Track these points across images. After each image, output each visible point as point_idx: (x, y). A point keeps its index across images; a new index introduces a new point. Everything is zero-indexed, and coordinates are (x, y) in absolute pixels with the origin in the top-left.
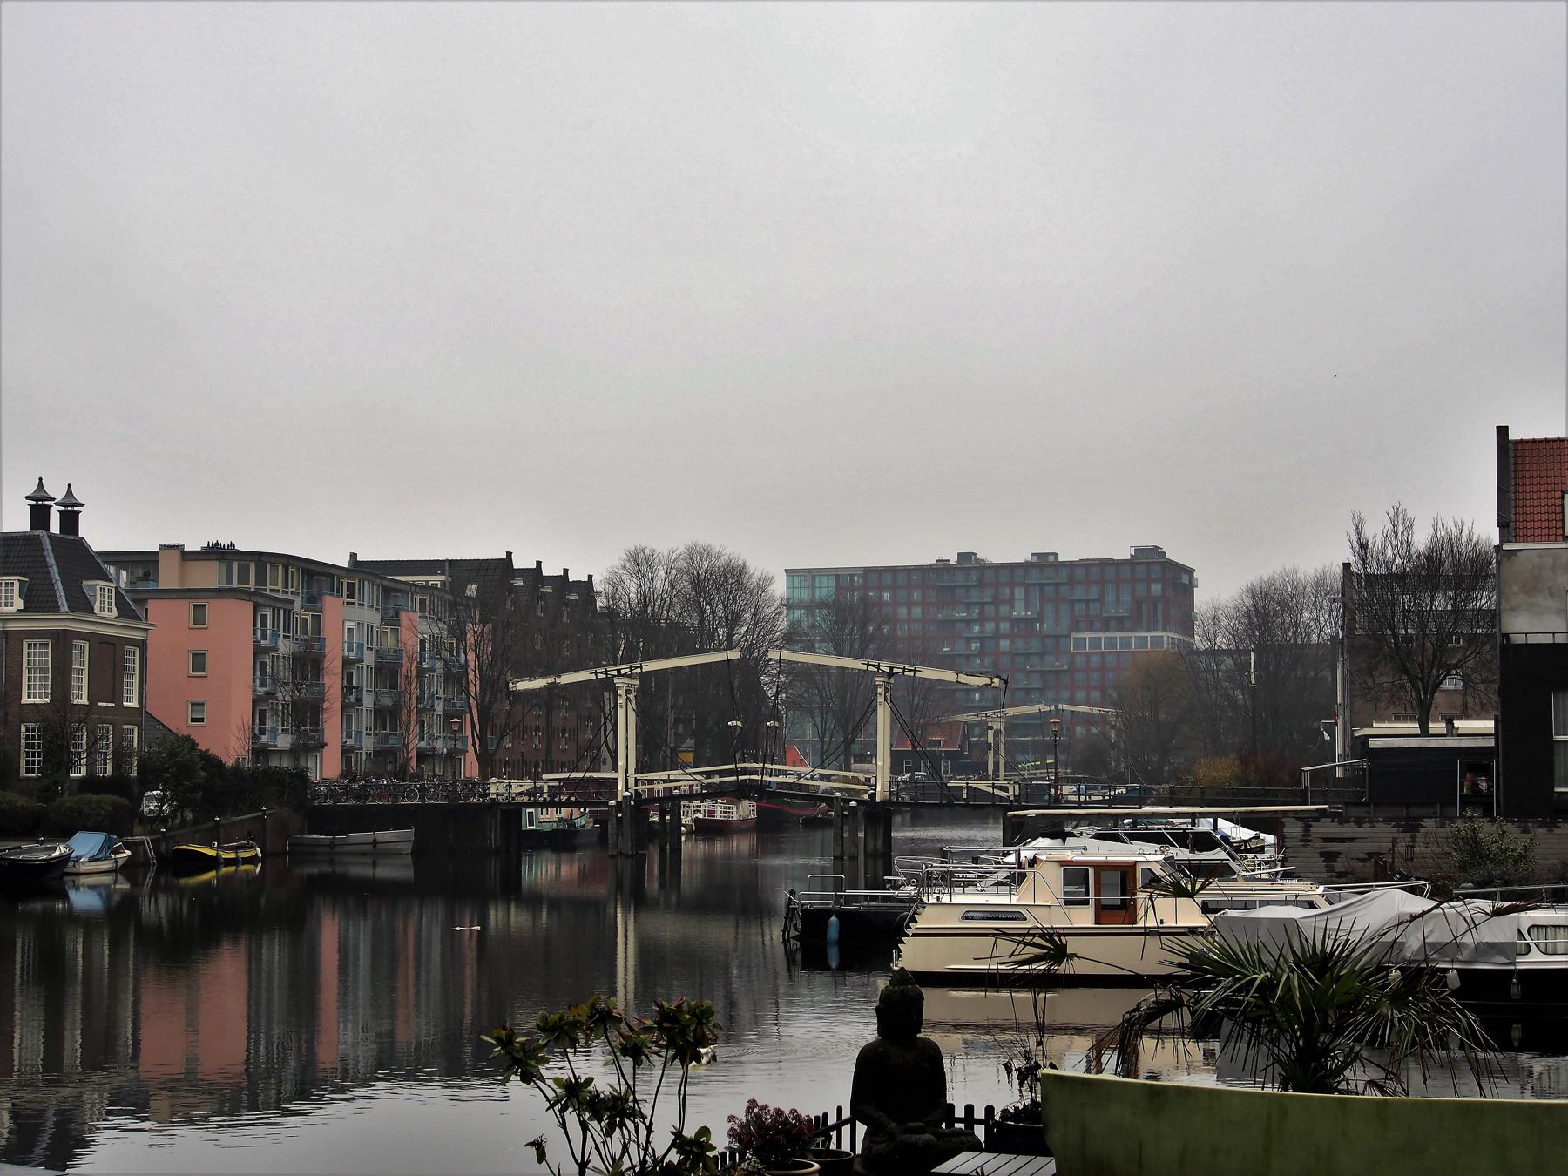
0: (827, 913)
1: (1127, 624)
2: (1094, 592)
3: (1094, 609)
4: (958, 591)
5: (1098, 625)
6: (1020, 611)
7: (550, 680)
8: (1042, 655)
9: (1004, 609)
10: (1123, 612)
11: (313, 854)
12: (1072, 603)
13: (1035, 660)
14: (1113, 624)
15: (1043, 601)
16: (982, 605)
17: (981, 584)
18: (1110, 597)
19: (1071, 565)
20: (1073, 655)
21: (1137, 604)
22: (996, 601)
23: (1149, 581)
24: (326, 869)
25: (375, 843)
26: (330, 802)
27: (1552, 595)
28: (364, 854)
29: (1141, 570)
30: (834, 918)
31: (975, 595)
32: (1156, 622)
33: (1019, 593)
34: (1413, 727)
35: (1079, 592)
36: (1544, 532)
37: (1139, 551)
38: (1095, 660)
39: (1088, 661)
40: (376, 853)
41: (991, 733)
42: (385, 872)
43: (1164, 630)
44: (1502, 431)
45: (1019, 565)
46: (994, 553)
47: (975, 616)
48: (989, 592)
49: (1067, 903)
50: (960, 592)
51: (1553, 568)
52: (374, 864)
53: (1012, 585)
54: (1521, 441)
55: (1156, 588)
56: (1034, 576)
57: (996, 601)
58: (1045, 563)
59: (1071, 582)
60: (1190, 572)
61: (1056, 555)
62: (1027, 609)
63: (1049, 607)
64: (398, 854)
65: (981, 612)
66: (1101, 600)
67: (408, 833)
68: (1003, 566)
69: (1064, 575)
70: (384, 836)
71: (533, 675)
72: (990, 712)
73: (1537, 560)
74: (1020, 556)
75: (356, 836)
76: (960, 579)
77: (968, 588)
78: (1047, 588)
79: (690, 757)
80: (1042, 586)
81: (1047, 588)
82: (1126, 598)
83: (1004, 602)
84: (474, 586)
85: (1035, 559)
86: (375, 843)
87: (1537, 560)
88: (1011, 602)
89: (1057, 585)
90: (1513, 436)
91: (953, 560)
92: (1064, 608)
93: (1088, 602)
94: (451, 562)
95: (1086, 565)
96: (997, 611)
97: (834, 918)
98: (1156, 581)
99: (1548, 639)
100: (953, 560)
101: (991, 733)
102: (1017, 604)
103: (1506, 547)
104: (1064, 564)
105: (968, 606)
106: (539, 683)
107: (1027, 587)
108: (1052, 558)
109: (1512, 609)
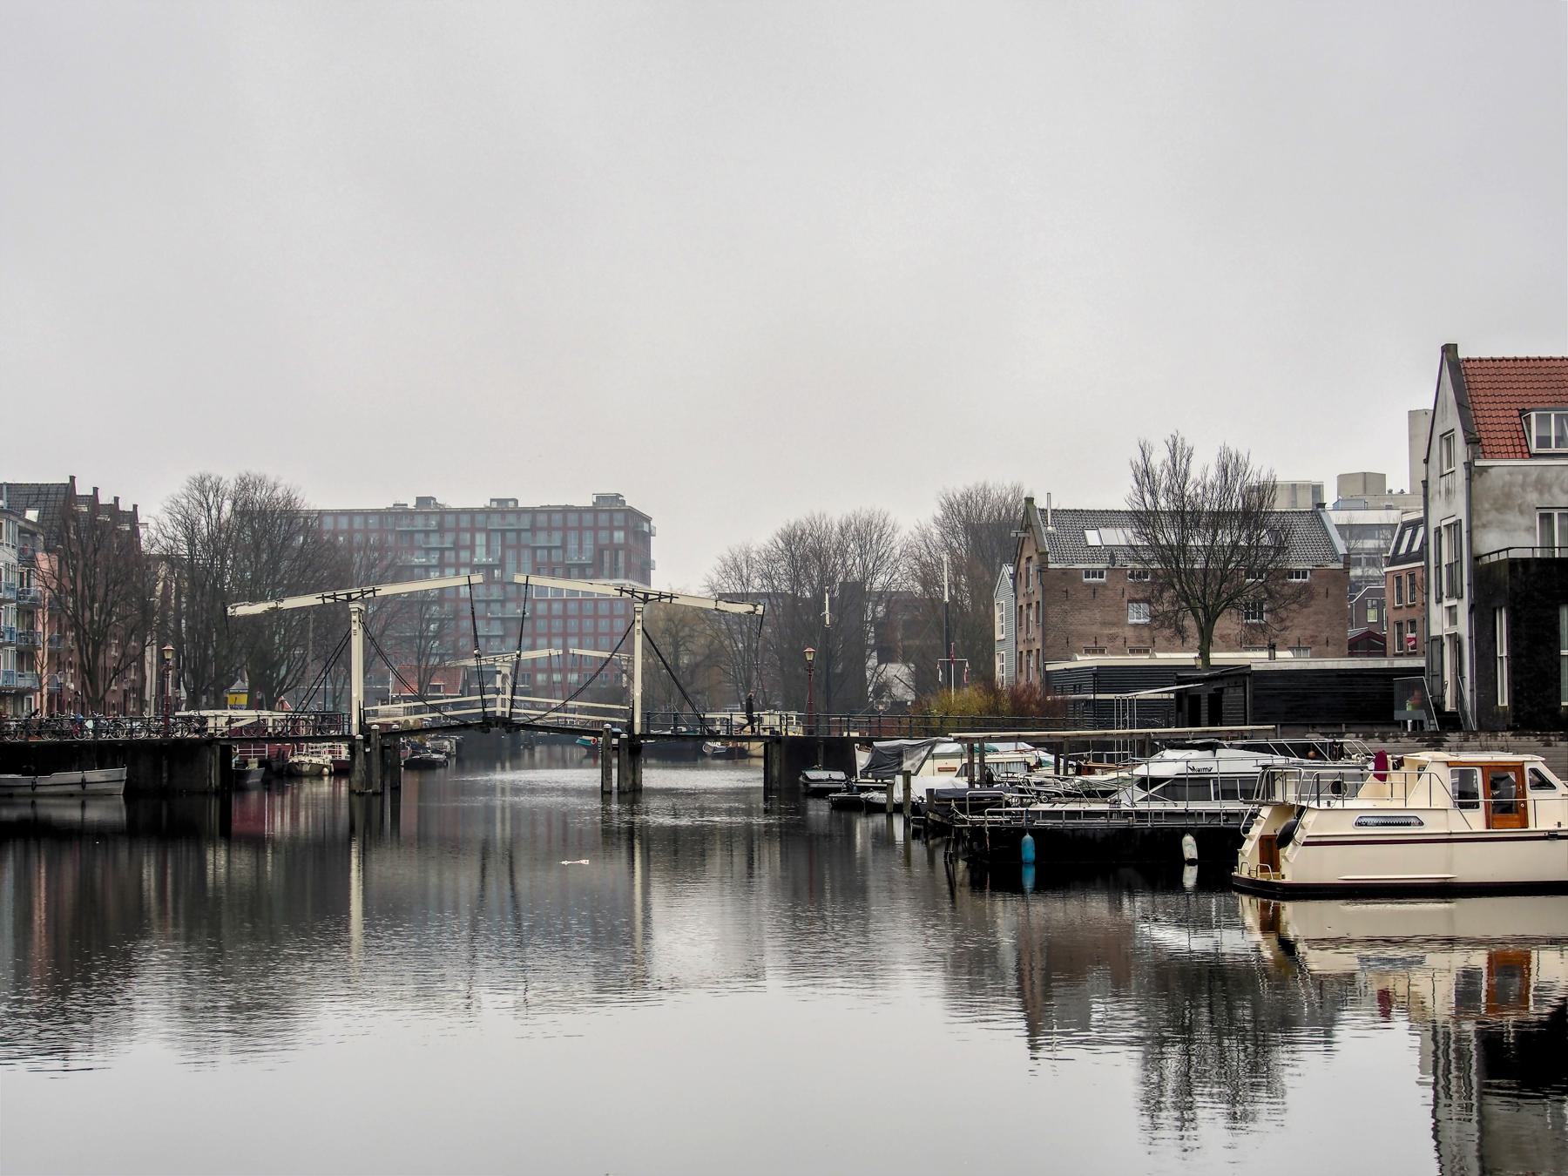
0: (1021, 832)
1: (589, 571)
2: (556, 540)
3: (557, 556)
4: (417, 536)
5: (560, 571)
6: (481, 557)
7: (272, 604)
8: (503, 602)
9: (464, 555)
10: (585, 559)
11: (11, 795)
12: (535, 549)
13: (496, 607)
14: (575, 571)
15: (504, 546)
16: (442, 550)
17: (441, 530)
18: (573, 545)
19: (533, 512)
20: (535, 602)
21: (599, 551)
22: (457, 547)
23: (612, 529)
24: (26, 812)
25: (83, 783)
26: (143, 735)
27: (1521, 512)
28: (71, 795)
29: (603, 518)
30: (1028, 837)
31: (434, 541)
32: (616, 570)
33: (480, 539)
34: (1265, 654)
35: (541, 539)
36: (1511, 449)
37: (601, 498)
38: (557, 608)
39: (550, 608)
40: (85, 795)
41: (499, 677)
42: (95, 814)
43: (626, 577)
44: (1449, 350)
45: (481, 511)
46: (454, 498)
47: (434, 562)
48: (448, 540)
49: (1462, 806)
50: (419, 537)
51: (1523, 486)
52: (83, 806)
53: (473, 530)
54: (1468, 360)
55: (619, 536)
56: (496, 521)
57: (457, 547)
58: (503, 508)
59: (533, 529)
60: (648, 520)
61: (516, 501)
62: (488, 553)
63: (510, 554)
64: (109, 795)
65: (442, 558)
66: (563, 547)
67: (121, 773)
68: (464, 511)
69: (526, 522)
70: (95, 776)
71: (254, 599)
72: (498, 657)
73: (1507, 478)
74: (481, 502)
75: (58, 777)
76: (419, 523)
77: (427, 533)
78: (508, 535)
79: (244, 699)
80: (503, 532)
81: (508, 535)
82: (588, 544)
83: (465, 548)
84: (36, 513)
85: (495, 505)
86: (83, 783)
87: (1507, 478)
88: (472, 548)
89: (519, 531)
90: (1462, 355)
91: (411, 505)
92: (526, 554)
93: (549, 549)
94: (9, 486)
95: (549, 511)
96: (457, 556)
97: (1028, 837)
98: (619, 528)
99: (1528, 554)
100: (411, 505)
101: (499, 677)
102: (478, 550)
103: (1477, 463)
104: (525, 511)
105: (428, 551)
106: (259, 608)
107: (489, 532)
108: (511, 504)
109: (1484, 526)
